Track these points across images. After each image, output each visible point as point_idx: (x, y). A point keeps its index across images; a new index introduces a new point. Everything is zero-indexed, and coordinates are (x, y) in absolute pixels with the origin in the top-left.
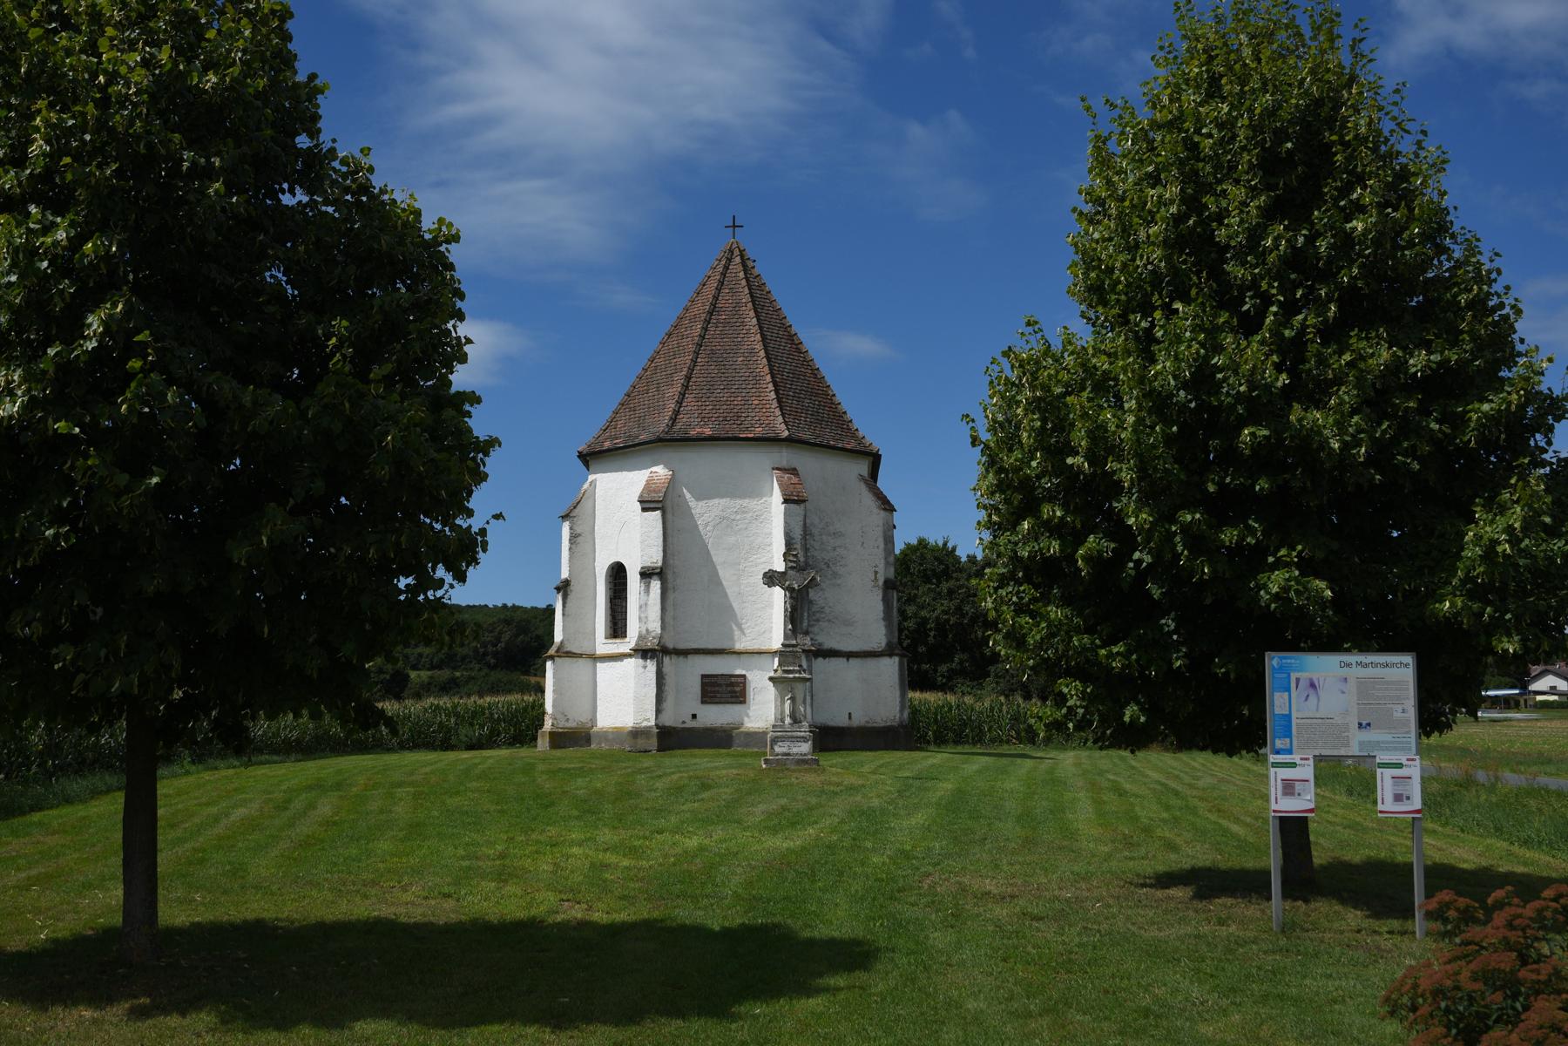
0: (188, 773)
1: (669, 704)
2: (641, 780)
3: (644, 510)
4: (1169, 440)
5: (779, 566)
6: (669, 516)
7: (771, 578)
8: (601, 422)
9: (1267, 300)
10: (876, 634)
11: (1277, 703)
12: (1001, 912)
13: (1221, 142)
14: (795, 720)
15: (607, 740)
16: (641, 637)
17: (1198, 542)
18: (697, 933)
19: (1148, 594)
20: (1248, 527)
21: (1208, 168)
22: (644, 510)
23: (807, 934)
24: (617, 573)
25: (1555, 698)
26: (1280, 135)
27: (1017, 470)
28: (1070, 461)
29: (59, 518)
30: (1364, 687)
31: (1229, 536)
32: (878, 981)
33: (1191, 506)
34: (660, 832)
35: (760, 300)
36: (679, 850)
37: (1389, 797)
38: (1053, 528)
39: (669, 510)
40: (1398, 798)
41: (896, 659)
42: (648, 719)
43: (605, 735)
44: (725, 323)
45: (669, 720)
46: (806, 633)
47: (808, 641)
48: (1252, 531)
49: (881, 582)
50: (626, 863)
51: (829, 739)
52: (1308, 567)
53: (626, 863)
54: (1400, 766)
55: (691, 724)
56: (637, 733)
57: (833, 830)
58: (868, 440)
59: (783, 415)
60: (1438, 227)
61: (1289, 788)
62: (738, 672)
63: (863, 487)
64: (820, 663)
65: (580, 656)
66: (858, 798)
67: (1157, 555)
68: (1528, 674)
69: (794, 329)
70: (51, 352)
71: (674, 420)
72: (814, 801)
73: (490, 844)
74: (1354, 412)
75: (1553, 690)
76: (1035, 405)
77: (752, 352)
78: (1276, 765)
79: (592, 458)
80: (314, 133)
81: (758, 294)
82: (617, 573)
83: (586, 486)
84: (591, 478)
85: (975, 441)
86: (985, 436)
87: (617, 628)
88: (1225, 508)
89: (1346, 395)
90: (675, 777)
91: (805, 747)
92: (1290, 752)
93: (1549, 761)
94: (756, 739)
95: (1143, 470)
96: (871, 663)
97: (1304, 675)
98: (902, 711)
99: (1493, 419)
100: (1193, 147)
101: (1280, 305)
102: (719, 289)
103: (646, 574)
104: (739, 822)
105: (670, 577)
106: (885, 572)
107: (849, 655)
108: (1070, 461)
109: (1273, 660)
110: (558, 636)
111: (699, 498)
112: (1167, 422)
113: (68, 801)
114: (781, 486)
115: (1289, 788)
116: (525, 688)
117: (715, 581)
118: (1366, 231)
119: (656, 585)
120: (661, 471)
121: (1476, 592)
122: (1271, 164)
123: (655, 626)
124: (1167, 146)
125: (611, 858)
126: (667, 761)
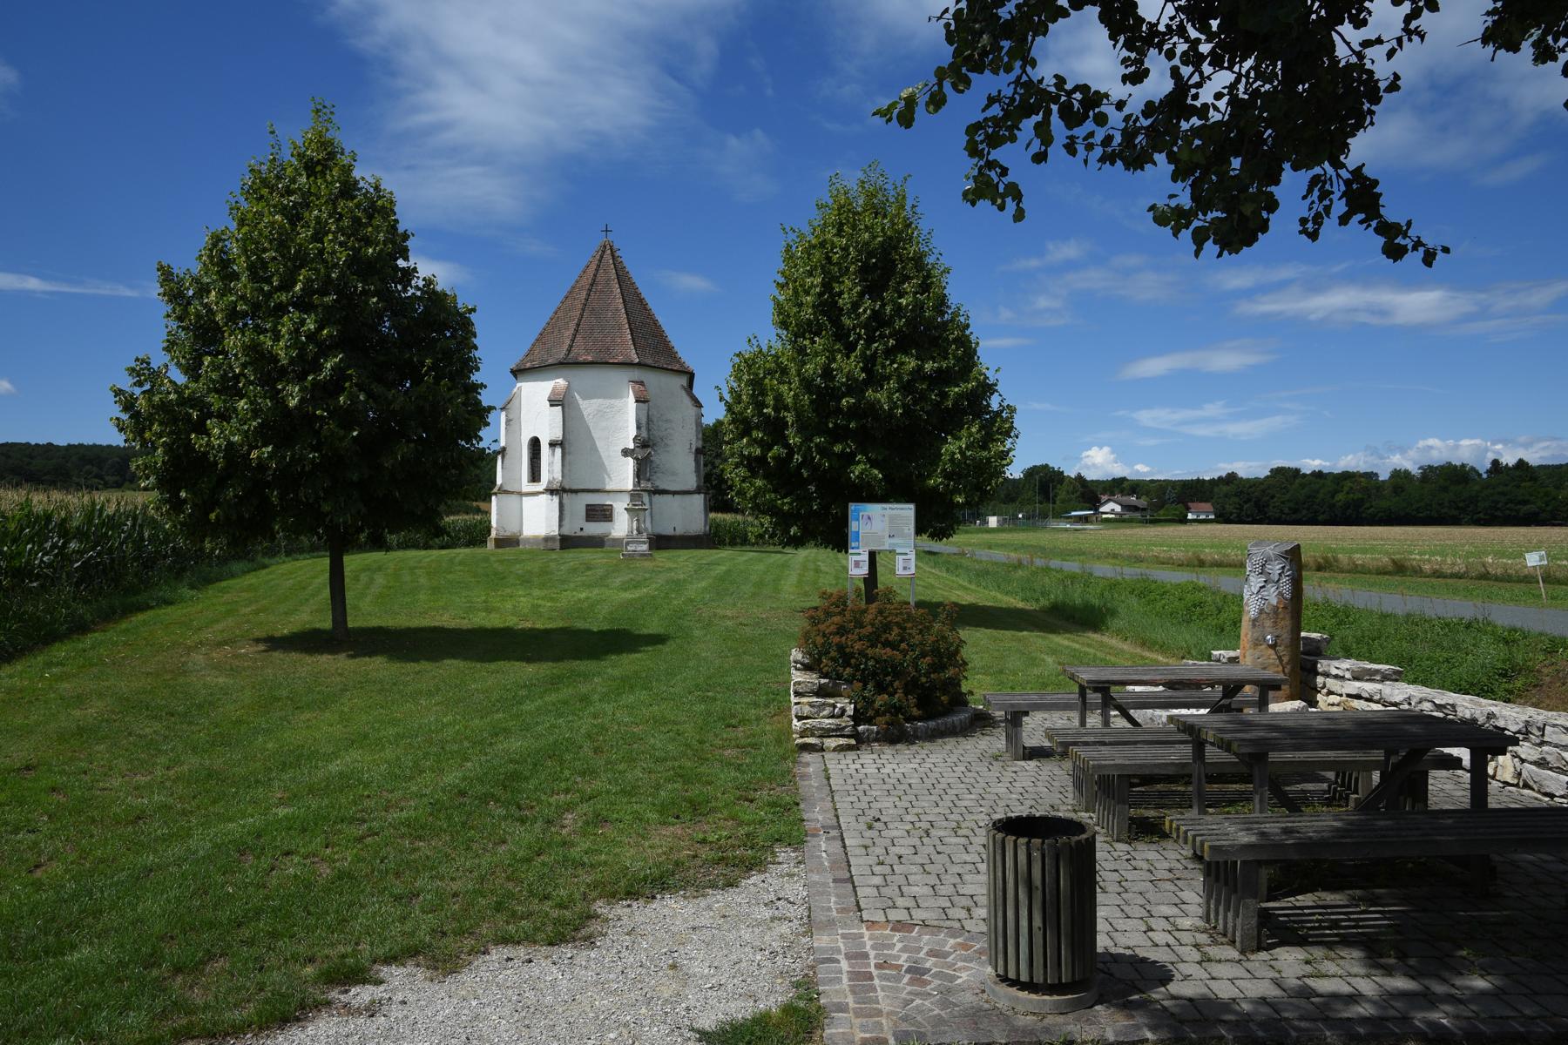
0: (284, 562)
1: (566, 522)
2: (553, 565)
3: (551, 405)
4: (812, 402)
5: (631, 446)
6: (566, 410)
7: (626, 452)
8: (525, 350)
9: (860, 337)
10: (691, 481)
11: (853, 526)
12: (729, 623)
13: (842, 257)
14: (639, 532)
15: (529, 543)
16: (549, 482)
17: (822, 450)
18: (588, 632)
19: (802, 474)
20: (847, 444)
21: (836, 269)
22: (551, 405)
23: (637, 632)
24: (535, 444)
25: (1113, 516)
26: (870, 255)
27: (741, 413)
28: (765, 411)
29: (314, 449)
30: (892, 519)
31: (838, 448)
32: (666, 648)
33: (820, 435)
34: (565, 591)
35: (622, 277)
36: (576, 599)
37: (901, 569)
38: (760, 442)
39: (566, 406)
40: (905, 568)
41: (702, 495)
42: (554, 530)
43: (528, 540)
44: (601, 291)
45: (566, 531)
46: (649, 480)
47: (649, 485)
48: (850, 447)
49: (694, 450)
50: (549, 604)
51: (660, 542)
52: (874, 464)
53: (549, 604)
54: (906, 554)
55: (579, 534)
56: (547, 539)
57: (657, 589)
58: (687, 364)
59: (636, 349)
60: (942, 302)
61: (857, 564)
62: (608, 503)
63: (684, 393)
64: (657, 498)
65: (512, 493)
66: (673, 574)
67: (804, 457)
68: (1099, 502)
69: (643, 296)
70: (310, 378)
71: (569, 351)
72: (647, 575)
73: (479, 597)
74: (897, 391)
75: (1112, 511)
76: (750, 383)
77: (617, 310)
78: (852, 554)
79: (518, 373)
80: (406, 259)
81: (621, 273)
82: (535, 444)
83: (515, 390)
84: (518, 385)
85: (721, 399)
86: (727, 397)
87: (535, 476)
88: (838, 435)
89: (893, 384)
90: (572, 564)
91: (645, 547)
92: (858, 548)
93: (1084, 554)
94: (617, 542)
95: (798, 416)
96: (687, 498)
97: (866, 513)
98: (705, 526)
99: (960, 396)
100: (828, 259)
101: (865, 340)
102: (597, 270)
103: (553, 445)
104: (607, 586)
105: (567, 446)
106: (696, 443)
107: (674, 493)
108: (765, 411)
109: (852, 506)
110: (499, 481)
111: (584, 398)
112: (811, 393)
113: (233, 576)
114: (634, 392)
115: (857, 564)
116: (478, 511)
117: (594, 449)
118: (907, 305)
119: (558, 451)
120: (561, 382)
121: (947, 476)
122: (864, 270)
123: (558, 476)
124: (817, 255)
125: (540, 602)
126: (566, 555)
